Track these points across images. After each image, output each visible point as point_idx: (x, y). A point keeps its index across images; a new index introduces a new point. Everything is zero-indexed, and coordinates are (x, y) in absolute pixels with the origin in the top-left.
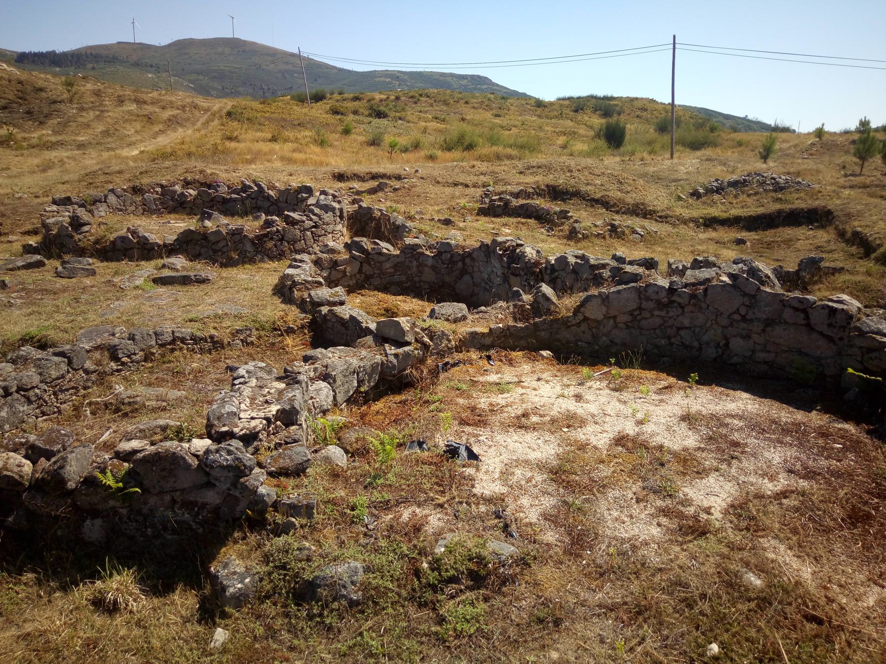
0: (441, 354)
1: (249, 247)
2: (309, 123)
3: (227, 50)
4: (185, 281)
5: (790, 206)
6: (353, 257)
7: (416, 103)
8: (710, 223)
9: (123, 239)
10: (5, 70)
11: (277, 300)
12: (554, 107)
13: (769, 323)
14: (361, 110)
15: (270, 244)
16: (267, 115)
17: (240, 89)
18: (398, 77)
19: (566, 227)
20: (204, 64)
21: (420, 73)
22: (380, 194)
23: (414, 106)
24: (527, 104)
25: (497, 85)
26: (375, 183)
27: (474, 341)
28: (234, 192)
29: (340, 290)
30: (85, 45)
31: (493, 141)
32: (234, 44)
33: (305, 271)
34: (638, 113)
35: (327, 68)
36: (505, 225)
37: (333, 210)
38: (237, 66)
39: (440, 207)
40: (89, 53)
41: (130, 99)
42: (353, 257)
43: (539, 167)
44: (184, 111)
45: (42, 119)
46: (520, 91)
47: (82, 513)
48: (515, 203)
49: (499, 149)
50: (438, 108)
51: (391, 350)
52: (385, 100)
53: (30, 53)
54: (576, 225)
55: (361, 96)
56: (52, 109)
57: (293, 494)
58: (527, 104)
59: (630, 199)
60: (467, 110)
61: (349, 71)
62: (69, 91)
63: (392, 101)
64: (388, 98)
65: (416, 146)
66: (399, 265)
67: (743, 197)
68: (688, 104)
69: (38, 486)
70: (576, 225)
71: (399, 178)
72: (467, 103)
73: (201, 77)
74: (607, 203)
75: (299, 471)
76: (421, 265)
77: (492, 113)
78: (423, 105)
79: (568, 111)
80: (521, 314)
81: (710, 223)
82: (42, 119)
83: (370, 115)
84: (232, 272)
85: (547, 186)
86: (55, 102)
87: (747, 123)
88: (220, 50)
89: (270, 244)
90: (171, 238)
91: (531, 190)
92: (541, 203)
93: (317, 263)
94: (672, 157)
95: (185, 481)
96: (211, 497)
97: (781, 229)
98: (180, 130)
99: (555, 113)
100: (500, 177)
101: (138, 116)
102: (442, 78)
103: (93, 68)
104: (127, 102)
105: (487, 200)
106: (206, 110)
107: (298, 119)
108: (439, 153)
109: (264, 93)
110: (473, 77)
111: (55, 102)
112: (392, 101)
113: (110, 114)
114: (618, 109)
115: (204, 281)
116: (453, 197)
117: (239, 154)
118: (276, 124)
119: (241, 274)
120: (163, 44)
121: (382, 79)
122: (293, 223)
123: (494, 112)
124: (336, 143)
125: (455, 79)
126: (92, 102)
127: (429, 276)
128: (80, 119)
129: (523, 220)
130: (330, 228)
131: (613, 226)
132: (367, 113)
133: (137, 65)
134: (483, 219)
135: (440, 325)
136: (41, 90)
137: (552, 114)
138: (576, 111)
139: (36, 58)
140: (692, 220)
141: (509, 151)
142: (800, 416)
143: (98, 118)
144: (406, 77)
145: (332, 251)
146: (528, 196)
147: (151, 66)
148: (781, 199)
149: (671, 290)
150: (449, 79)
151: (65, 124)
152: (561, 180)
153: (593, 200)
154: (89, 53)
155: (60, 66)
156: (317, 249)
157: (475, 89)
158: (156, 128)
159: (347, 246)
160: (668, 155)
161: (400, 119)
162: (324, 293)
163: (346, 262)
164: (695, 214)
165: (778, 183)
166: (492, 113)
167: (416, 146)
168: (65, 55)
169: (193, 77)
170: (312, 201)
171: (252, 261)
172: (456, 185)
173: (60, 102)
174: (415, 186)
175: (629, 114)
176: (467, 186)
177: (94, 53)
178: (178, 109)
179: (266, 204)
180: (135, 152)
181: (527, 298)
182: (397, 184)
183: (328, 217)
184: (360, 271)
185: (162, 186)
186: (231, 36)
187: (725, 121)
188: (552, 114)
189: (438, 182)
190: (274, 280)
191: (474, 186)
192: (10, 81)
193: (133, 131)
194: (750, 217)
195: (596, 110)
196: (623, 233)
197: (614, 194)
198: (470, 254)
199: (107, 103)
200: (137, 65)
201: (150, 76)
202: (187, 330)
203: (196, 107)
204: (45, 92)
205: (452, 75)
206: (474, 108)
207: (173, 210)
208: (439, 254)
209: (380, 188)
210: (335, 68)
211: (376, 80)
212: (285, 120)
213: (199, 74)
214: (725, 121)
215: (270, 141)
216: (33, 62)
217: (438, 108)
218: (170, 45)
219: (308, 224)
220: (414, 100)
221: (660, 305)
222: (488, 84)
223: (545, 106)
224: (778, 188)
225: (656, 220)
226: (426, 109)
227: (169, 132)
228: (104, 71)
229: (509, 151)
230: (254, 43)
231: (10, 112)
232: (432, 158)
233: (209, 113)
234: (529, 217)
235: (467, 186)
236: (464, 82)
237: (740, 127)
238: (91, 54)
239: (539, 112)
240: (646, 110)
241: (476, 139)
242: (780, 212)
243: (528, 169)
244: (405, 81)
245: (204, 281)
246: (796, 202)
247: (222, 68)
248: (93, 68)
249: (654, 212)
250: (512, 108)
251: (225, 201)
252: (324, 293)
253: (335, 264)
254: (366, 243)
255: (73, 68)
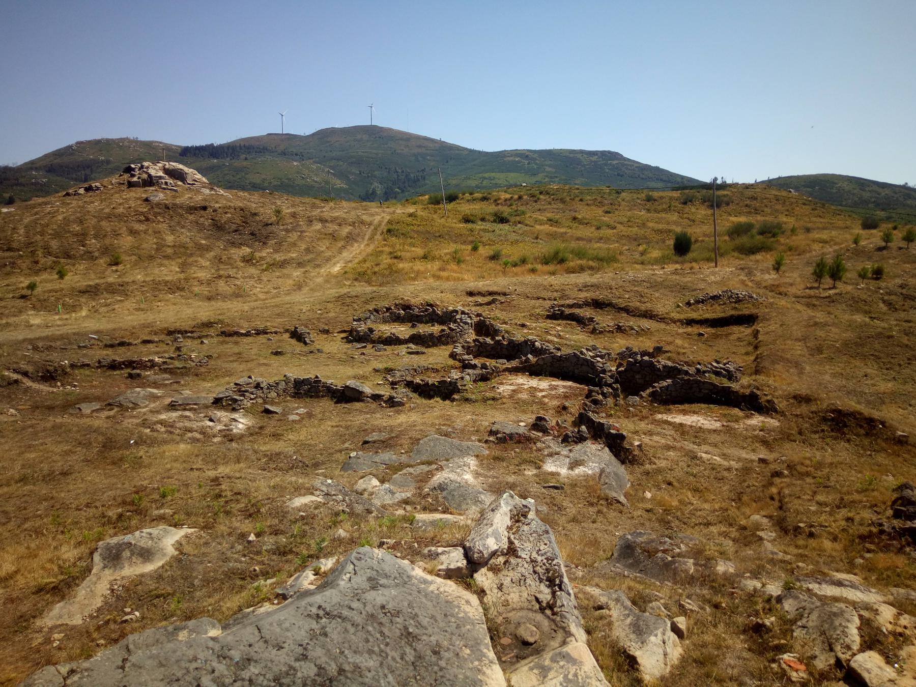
0: (497, 372)
1: (435, 340)
2: (446, 234)
3: (365, 137)
4: (417, 353)
5: (740, 313)
6: (476, 345)
7: (536, 201)
8: (690, 322)
9: (390, 337)
10: (222, 195)
11: (451, 360)
12: (664, 200)
13: (582, 365)
14: (487, 217)
15: (443, 339)
16: (415, 228)
17: (376, 173)
18: (527, 156)
19: (591, 327)
20: (343, 151)
21: (550, 151)
22: (493, 305)
23: (534, 204)
24: (638, 198)
25: (629, 160)
26: (490, 298)
27: (507, 370)
28: (421, 312)
29: (471, 356)
30: (239, 138)
31: (580, 254)
32: (373, 133)
33: (459, 350)
34: (748, 202)
35: (458, 150)
36: (559, 325)
37: (468, 324)
38: (374, 151)
39: (525, 314)
40: (242, 145)
41: (316, 219)
42: (476, 345)
43: (592, 286)
44: (354, 226)
45: (263, 240)
46: (653, 165)
47: (431, 390)
48: (568, 311)
49: (583, 262)
50: (555, 206)
51: (484, 370)
52: (509, 200)
53: (192, 147)
54: (596, 326)
55: (489, 196)
56: (268, 232)
57: (464, 388)
58: (638, 198)
59: (643, 308)
60: (581, 207)
61: (479, 152)
62: (277, 217)
63: (515, 201)
64: (512, 198)
65: (524, 261)
66: (493, 347)
67: (716, 306)
68: (838, 173)
69: (424, 385)
70: (596, 326)
71: (505, 294)
72: (581, 200)
73: (341, 163)
74: (628, 310)
75: (465, 385)
76: (502, 348)
77: (603, 209)
78: (543, 203)
79: (677, 204)
80: (521, 363)
81: (690, 322)
82: (263, 240)
83: (495, 221)
84: (430, 350)
85: (592, 300)
86: (267, 225)
87: (906, 191)
88: (359, 137)
89: (443, 339)
90: (407, 337)
91: (581, 303)
92: (586, 313)
93: (463, 347)
94: (716, 266)
95: (447, 385)
96: (451, 388)
97: (731, 327)
98: (356, 245)
99: (664, 206)
100: (567, 293)
101: (326, 234)
102: (572, 155)
103: (246, 159)
104: (315, 222)
105: (552, 310)
106: (370, 224)
107: (439, 231)
108: (539, 267)
109: (398, 176)
110: (603, 153)
111: (267, 225)
112: (515, 201)
113: (307, 234)
114: (725, 199)
115: (423, 353)
116: (534, 308)
117: (406, 273)
118: (423, 236)
119: (400, 347)
120: (307, 134)
121: (511, 159)
122: (452, 330)
123: (605, 208)
124: (468, 258)
125: (585, 156)
126: (291, 223)
127: (505, 352)
128: (289, 239)
129: (569, 322)
130: (466, 332)
131: (618, 326)
132: (492, 219)
133: (284, 154)
134: (549, 321)
135: (498, 365)
136: (255, 214)
137: (660, 208)
138: (685, 203)
139: (197, 151)
140: (679, 320)
141: (591, 263)
142: (578, 385)
143: (301, 238)
144: (536, 156)
145: (468, 342)
146: (580, 306)
147: (296, 155)
148: (736, 308)
149: (561, 357)
150: (579, 156)
151: (280, 244)
152: (600, 295)
153: (620, 308)
154: (242, 145)
155: (217, 158)
156: (461, 340)
157: (606, 165)
158: (340, 244)
159: (474, 340)
160: (714, 264)
161: (519, 223)
162: (466, 357)
163: (473, 347)
164: (682, 317)
165: (738, 297)
166: (603, 209)
167: (524, 261)
168: (221, 147)
169: (333, 163)
170: (458, 317)
171: (436, 346)
172: (538, 299)
173: (271, 224)
174: (513, 300)
175: (737, 204)
176: (545, 299)
177: (247, 144)
178: (350, 225)
179: (437, 318)
180: (337, 269)
181: (524, 358)
182: (502, 299)
183: (466, 327)
184: (478, 350)
185: (386, 308)
186: (368, 123)
187: (880, 190)
188: (660, 208)
189: (528, 297)
190: (448, 353)
191: (549, 300)
192: (235, 209)
193: (325, 247)
194: (714, 319)
195: (705, 202)
196: (625, 330)
197: (635, 304)
198: (520, 344)
199: (301, 223)
200: (284, 154)
201: (295, 164)
202: (430, 366)
203: (362, 222)
204: (259, 216)
205: (582, 152)
206: (587, 205)
207: (394, 321)
208: (509, 344)
209: (493, 301)
210: (466, 149)
211: (505, 159)
212: (429, 232)
213: (338, 160)
214: (880, 190)
215: (423, 258)
216: (195, 154)
217: (555, 206)
218: (313, 134)
219: (458, 330)
220: (535, 199)
221: (558, 361)
222: (617, 159)
223: (655, 200)
224: (739, 301)
225: (657, 321)
226: (545, 207)
227: (348, 247)
228: (255, 161)
229: (591, 263)
230: (390, 129)
231: (240, 234)
232: (533, 271)
233: (372, 227)
234: (573, 320)
235: (545, 299)
236: (594, 158)
237: (896, 196)
238: (244, 146)
239: (649, 205)
240: (756, 199)
241: (567, 255)
242: (732, 316)
243: (585, 287)
244: (534, 159)
245: (423, 353)
246: (744, 310)
247: (360, 153)
248: (246, 159)
249: (657, 315)
250: (623, 203)
251: (418, 316)
252: (466, 357)
253: (469, 347)
254: (481, 339)
255: (228, 159)
